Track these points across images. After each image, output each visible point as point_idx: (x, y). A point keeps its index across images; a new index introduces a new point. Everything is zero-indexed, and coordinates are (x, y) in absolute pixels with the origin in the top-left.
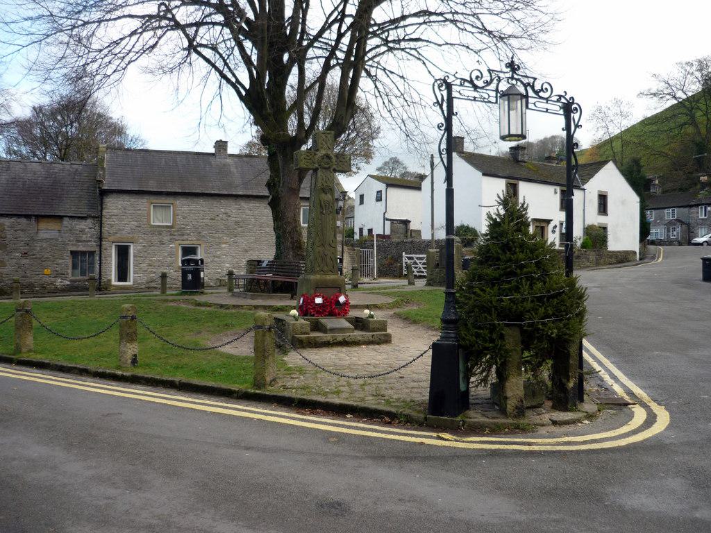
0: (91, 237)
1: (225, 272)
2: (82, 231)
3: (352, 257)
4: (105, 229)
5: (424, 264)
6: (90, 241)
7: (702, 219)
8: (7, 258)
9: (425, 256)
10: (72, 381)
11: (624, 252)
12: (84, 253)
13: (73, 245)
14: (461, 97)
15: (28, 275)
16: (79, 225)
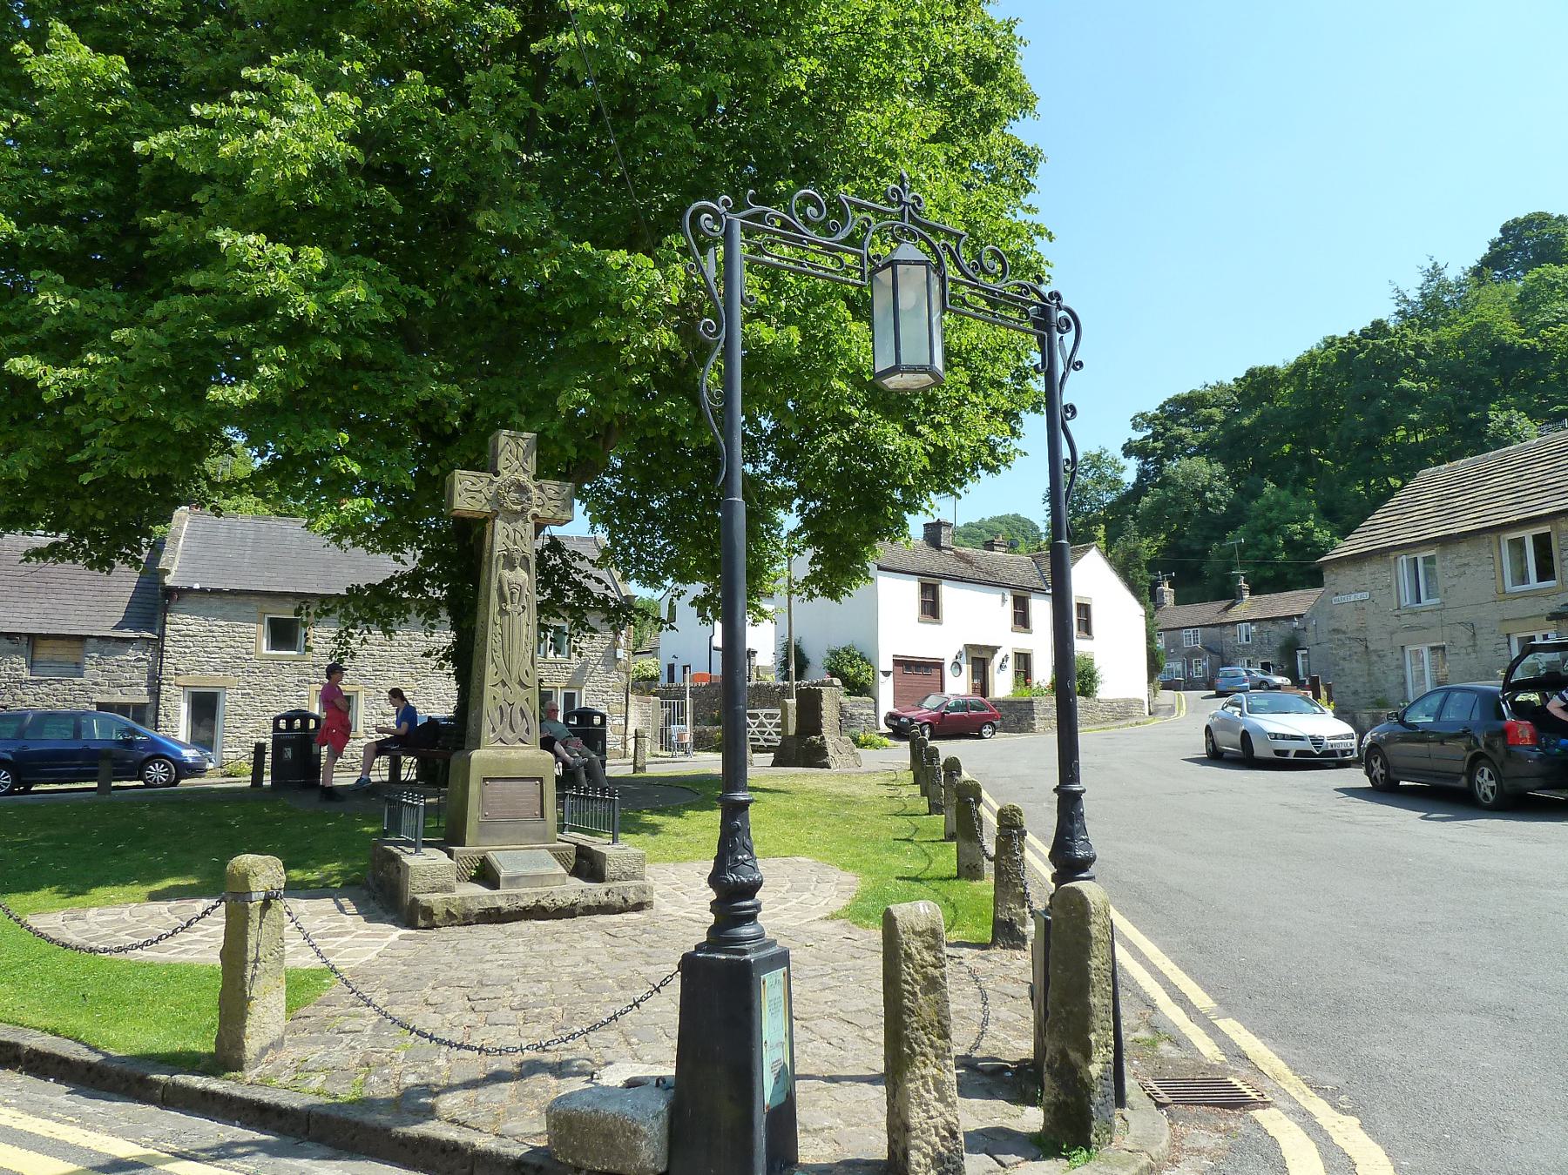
3: (644, 713)
5: (777, 725)
7: (1244, 646)
9: (778, 711)
10: (1452, 532)
13: (101, 692)
14: (969, 573)
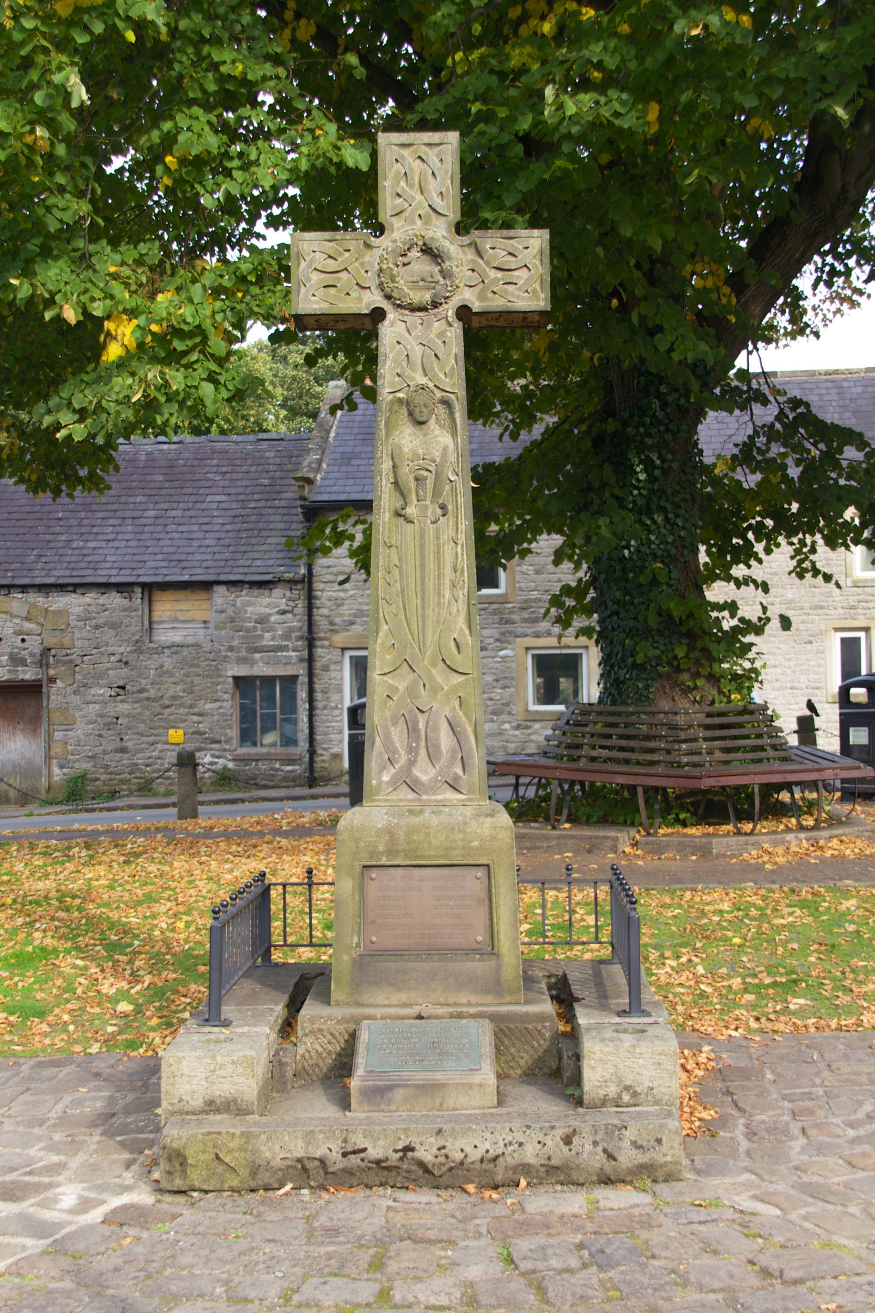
0: (286, 636)
1: (171, 757)
2: (263, 620)
4: (321, 612)
6: (282, 648)
8: (76, 700)
11: (377, 204)
12: (269, 681)
15: (130, 744)
16: (254, 604)
